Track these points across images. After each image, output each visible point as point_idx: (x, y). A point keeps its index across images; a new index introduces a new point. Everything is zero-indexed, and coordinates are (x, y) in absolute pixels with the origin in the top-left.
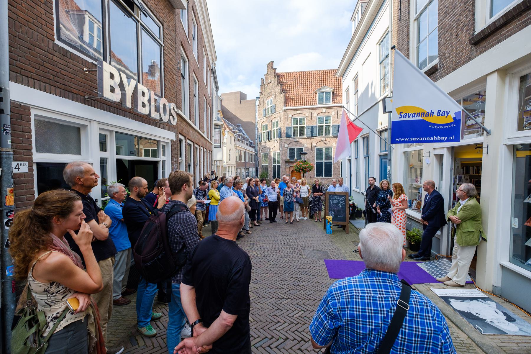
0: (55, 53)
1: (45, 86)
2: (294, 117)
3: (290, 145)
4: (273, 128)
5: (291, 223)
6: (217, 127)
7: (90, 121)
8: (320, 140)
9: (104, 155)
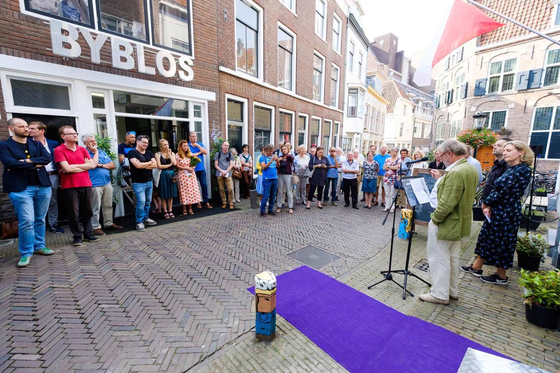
0: (22, 22)
1: (13, 52)
2: (494, 61)
3: (479, 108)
4: (457, 84)
5: (308, 209)
6: (353, 91)
7: (73, 80)
8: (546, 93)
9: (198, 119)
